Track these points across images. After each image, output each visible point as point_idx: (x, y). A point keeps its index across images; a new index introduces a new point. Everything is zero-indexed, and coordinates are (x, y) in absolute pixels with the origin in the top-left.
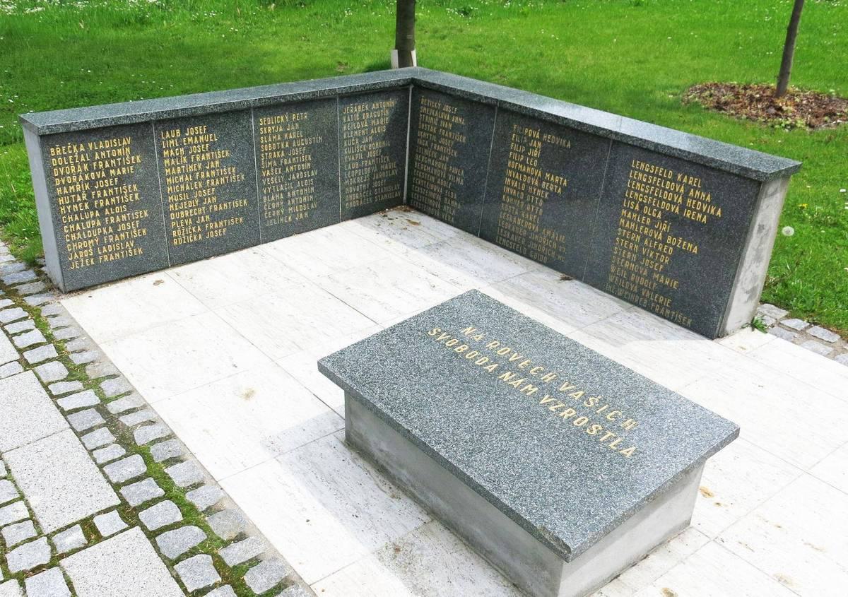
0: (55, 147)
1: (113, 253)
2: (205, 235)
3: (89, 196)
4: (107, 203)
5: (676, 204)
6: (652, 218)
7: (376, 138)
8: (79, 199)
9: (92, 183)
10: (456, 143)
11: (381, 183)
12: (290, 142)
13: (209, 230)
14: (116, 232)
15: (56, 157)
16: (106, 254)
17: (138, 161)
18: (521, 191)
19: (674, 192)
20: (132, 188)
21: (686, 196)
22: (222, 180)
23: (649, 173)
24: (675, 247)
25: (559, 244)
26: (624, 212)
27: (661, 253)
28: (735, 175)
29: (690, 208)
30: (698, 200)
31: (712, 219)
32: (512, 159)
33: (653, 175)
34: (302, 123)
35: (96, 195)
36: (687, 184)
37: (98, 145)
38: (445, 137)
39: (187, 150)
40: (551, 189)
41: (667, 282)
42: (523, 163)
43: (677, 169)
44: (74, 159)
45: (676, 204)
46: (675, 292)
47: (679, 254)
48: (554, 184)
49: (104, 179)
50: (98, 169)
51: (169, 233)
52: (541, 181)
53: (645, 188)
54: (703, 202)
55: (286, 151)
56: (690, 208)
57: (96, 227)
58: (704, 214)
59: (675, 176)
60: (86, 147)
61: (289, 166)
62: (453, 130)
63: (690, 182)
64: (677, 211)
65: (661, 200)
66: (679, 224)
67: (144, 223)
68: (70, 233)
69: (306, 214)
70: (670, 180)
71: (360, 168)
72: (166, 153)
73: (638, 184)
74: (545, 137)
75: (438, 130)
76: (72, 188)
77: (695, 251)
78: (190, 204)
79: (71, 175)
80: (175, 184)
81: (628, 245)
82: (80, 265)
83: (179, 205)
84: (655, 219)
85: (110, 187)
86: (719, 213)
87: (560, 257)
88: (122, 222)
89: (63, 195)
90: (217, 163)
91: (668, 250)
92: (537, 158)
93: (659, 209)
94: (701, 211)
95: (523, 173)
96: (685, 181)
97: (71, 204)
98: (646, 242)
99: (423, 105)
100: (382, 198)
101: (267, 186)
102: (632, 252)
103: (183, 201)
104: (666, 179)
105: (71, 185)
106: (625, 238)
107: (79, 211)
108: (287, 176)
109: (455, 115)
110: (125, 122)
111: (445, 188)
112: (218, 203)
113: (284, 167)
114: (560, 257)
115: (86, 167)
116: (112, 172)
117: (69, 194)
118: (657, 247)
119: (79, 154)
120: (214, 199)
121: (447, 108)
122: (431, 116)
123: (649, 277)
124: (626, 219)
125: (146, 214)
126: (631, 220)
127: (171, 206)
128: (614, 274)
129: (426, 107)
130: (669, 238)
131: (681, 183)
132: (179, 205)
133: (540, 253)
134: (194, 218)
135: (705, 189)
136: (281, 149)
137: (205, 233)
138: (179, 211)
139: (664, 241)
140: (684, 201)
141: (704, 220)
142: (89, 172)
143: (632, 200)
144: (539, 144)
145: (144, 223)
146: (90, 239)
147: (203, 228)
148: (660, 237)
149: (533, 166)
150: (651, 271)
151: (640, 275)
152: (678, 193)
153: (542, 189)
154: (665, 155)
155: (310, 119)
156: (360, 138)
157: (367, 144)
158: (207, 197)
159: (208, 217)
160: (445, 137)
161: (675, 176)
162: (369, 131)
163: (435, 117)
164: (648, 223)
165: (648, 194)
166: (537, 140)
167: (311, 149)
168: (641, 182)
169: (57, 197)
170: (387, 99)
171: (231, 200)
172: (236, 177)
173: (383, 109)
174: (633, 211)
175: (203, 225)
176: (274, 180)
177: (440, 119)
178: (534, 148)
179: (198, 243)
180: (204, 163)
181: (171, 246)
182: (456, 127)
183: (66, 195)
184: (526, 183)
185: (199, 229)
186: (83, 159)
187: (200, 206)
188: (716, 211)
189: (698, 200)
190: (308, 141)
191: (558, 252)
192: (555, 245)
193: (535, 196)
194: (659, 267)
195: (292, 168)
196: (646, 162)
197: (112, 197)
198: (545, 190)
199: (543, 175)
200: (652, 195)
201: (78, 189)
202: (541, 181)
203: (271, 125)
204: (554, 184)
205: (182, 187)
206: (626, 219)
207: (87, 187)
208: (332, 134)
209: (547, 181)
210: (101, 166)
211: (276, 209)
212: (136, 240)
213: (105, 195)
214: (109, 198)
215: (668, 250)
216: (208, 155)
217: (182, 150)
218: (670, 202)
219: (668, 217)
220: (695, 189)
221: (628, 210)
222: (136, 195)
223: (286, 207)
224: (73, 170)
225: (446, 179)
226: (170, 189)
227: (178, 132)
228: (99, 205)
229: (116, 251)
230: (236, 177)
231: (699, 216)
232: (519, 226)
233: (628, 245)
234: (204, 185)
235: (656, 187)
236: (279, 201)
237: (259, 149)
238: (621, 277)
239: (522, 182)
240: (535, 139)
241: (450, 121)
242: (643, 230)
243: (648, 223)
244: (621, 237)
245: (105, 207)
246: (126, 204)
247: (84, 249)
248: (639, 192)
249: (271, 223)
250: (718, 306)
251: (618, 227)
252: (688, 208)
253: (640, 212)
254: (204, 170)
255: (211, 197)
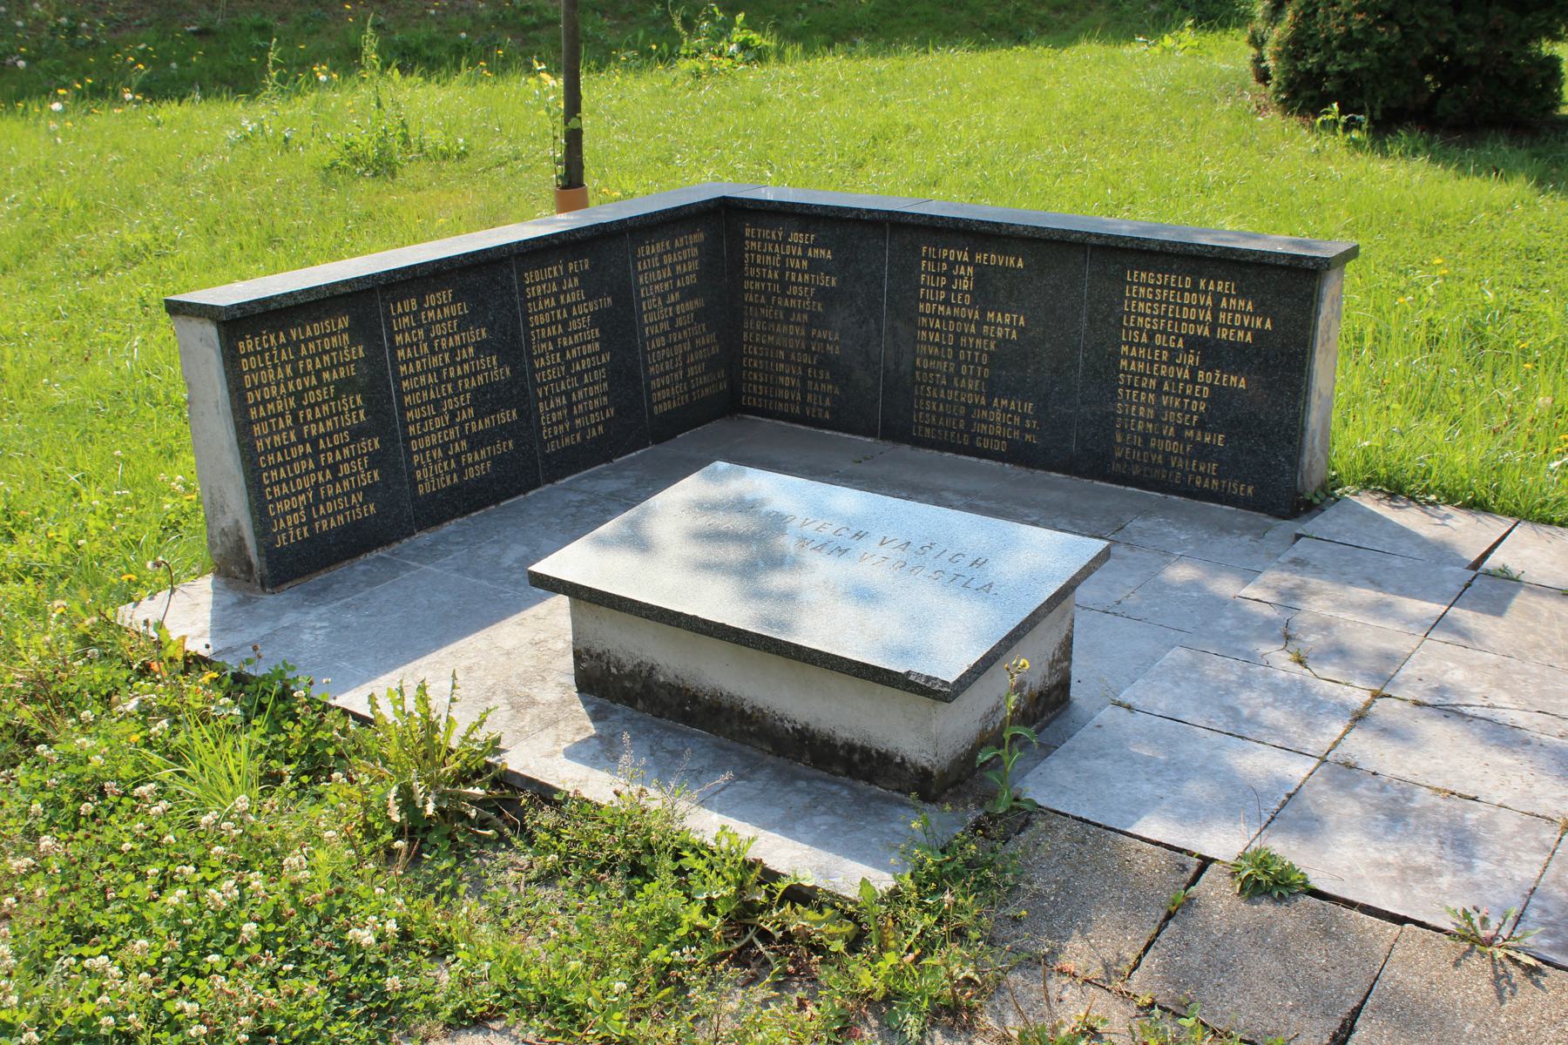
0: (244, 340)
1: (335, 514)
2: (461, 474)
3: (295, 419)
4: (322, 430)
5: (1203, 323)
6: (1168, 349)
7: (688, 294)
8: (282, 425)
9: (299, 396)
10: (820, 289)
11: (699, 369)
12: (569, 307)
13: (468, 466)
14: (336, 479)
15: (247, 355)
16: (324, 517)
17: (361, 354)
18: (947, 346)
19: (1198, 306)
20: (355, 402)
21: (1216, 309)
22: (480, 378)
23: (1154, 286)
24: (1211, 386)
25: (1024, 417)
26: (1125, 349)
27: (1192, 398)
28: (1283, 267)
29: (1225, 326)
30: (1234, 312)
31: (1259, 334)
32: (924, 300)
33: (1162, 287)
34: (582, 276)
35: (305, 417)
36: (1215, 293)
37: (304, 332)
38: (796, 284)
39: (428, 332)
40: (1000, 334)
41: (1207, 439)
42: (946, 302)
43: (1197, 275)
44: (271, 359)
45: (1203, 323)
46: (1221, 450)
47: (1219, 395)
48: (1004, 326)
49: (314, 389)
50: (306, 373)
51: (412, 475)
52: (979, 324)
53: (1152, 308)
54: (1243, 313)
55: (565, 323)
56: (1225, 326)
57: (308, 472)
58: (1247, 330)
59: (1195, 285)
60: (288, 335)
61: (570, 348)
62: (810, 270)
63: (1219, 289)
64: (1206, 333)
65: (1180, 321)
66: (1211, 352)
67: (375, 460)
68: (271, 485)
69: (600, 428)
70: (1189, 290)
71: (668, 345)
72: (398, 338)
73: (1141, 305)
74: (978, 257)
75: (782, 275)
76: (270, 407)
77: (1242, 385)
78: (439, 423)
79: (269, 385)
80: (415, 391)
81: (1138, 397)
82: (288, 539)
83: (422, 426)
84: (1176, 350)
85: (324, 401)
86: (1268, 325)
87: (1028, 437)
88: (343, 461)
89: (260, 420)
90: (471, 350)
91: (1201, 391)
92: (968, 292)
93: (1179, 335)
94: (1242, 327)
95: (947, 318)
96: (1211, 287)
97: (271, 434)
98: (1166, 388)
99: (750, 239)
100: (333, 524)
101: (543, 384)
102: (1146, 405)
103: (427, 418)
104: (1183, 290)
105: (269, 401)
106: (1132, 387)
107: (284, 446)
108: (568, 364)
109: (813, 246)
110: (343, 290)
111: (805, 367)
112: (478, 416)
113: (563, 351)
114: (1028, 437)
115: (289, 371)
116: (326, 375)
117: (267, 418)
118: (1184, 390)
119: (279, 347)
120: (471, 411)
121: (796, 237)
122: (767, 253)
123: (1179, 436)
124: (1130, 359)
125: (377, 445)
126: (1137, 359)
127: (411, 429)
128: (1122, 445)
129: (756, 240)
130: (1201, 374)
131: (1206, 292)
132: (422, 426)
133: (995, 437)
134: (445, 446)
135: (1241, 294)
136: (556, 323)
137: (461, 470)
138: (423, 435)
139: (1193, 380)
140: (1215, 317)
141: (1249, 338)
142: (294, 378)
143: (1133, 329)
144: (970, 270)
145: (375, 460)
146: (301, 492)
147: (458, 462)
148: (1187, 376)
149: (964, 305)
150: (1180, 429)
151: (1164, 438)
152: (1204, 307)
153: (984, 338)
154: (1177, 255)
155: (593, 268)
156: (664, 296)
157: (674, 305)
158: (460, 409)
159: (464, 443)
160: (796, 284)
161: (1195, 285)
162: (675, 283)
163: (773, 254)
164: (1164, 358)
165: (1159, 317)
166: (966, 264)
167: (598, 319)
168: (1145, 300)
169: (252, 423)
170: (693, 232)
171: (494, 412)
172: (495, 370)
173: (687, 252)
174: (1139, 345)
175: (457, 456)
176: (552, 374)
177: (784, 257)
178: (962, 277)
179: (453, 488)
180: (452, 351)
181: (415, 497)
182: (816, 266)
183: (263, 419)
184: (955, 332)
185: (453, 465)
186: (284, 357)
187: (451, 425)
188: (1263, 323)
189: (1234, 312)
190: (592, 306)
191: (1024, 430)
192: (1017, 420)
193: (974, 349)
194: (1191, 420)
195: (329, 423)
196: (1148, 270)
197: (328, 417)
198: (988, 337)
199: (983, 314)
200: (1165, 317)
201: (280, 408)
202: (979, 324)
203: (541, 283)
204: (1004, 326)
205: (425, 394)
206: (1130, 359)
207: (292, 403)
208: (625, 297)
209: (990, 324)
210: (310, 367)
211: (559, 423)
212: (364, 489)
213: (318, 415)
214: (323, 420)
215: (1201, 391)
216: (457, 338)
217: (421, 332)
218: (1194, 322)
219: (1193, 343)
220: (1229, 296)
221: (1131, 344)
222: (362, 413)
223: (572, 418)
224: (272, 376)
225: (808, 350)
226: (407, 399)
227: (414, 302)
228: (309, 433)
229: (339, 512)
230: (495, 370)
231: (1241, 334)
232: (951, 403)
233: (1138, 397)
234: (455, 387)
235: (1169, 303)
236: (561, 408)
237: (527, 323)
238: (1134, 447)
239: (947, 332)
240: (961, 263)
241: (804, 256)
242: (1159, 370)
243: (1164, 358)
244: (1125, 386)
245: (319, 436)
246: (347, 428)
247: (293, 511)
248: (1144, 315)
249: (551, 448)
250: (1288, 457)
251: (1119, 372)
252: (1222, 326)
253: (1150, 345)
254: (453, 363)
255: (465, 408)
